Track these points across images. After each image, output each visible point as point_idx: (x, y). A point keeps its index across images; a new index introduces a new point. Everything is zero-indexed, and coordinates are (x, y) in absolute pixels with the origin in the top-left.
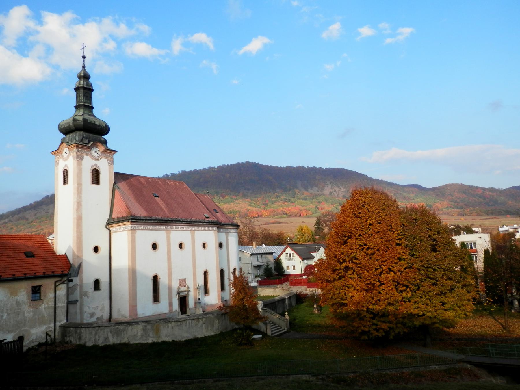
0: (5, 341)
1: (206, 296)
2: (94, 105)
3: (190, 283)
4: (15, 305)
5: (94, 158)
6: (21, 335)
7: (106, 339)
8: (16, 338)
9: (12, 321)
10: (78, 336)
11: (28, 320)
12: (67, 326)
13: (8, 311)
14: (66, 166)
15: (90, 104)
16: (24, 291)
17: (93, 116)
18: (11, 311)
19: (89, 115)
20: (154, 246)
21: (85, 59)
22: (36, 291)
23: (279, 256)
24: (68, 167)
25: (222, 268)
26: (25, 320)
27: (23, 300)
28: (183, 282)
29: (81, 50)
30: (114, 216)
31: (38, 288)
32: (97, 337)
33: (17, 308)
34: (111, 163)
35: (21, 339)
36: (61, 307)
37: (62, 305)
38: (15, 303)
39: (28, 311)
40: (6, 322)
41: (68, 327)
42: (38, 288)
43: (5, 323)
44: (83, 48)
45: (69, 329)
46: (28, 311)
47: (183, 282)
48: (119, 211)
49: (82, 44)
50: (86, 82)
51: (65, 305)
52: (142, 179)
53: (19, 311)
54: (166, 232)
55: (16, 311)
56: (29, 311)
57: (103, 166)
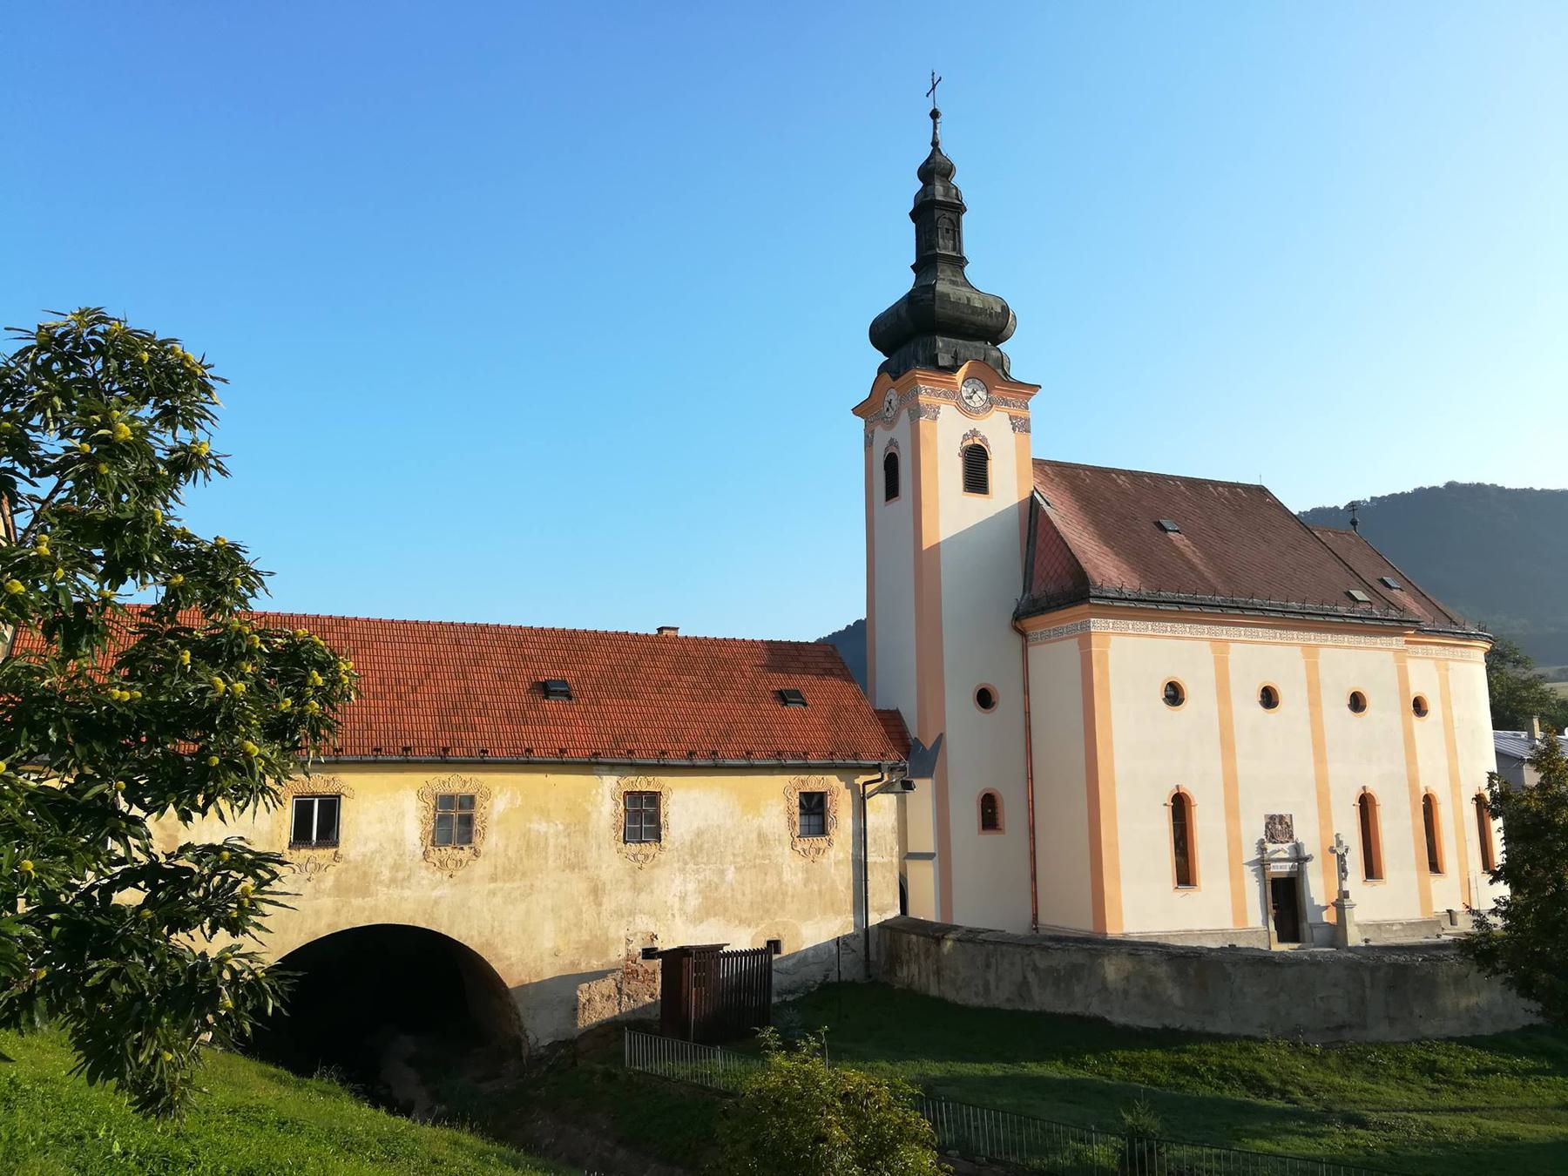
0: (726, 949)
1: (1001, 826)
2: (967, 251)
3: (1307, 834)
4: (755, 844)
5: (966, 410)
6: (775, 937)
7: (1023, 987)
8: (762, 945)
9: (748, 891)
10: (933, 964)
11: (790, 894)
12: (901, 927)
13: (738, 860)
14: (892, 442)
15: (954, 249)
16: (779, 805)
17: (967, 284)
18: (745, 860)
19: (954, 283)
20: (1174, 695)
21: (938, 120)
22: (814, 811)
23: (1410, 786)
24: (897, 447)
25: (979, 833)
26: (785, 894)
27: (776, 830)
28: (1278, 827)
29: (927, 96)
30: (1036, 593)
31: (816, 799)
32: (991, 977)
33: (761, 853)
34: (1021, 426)
35: (774, 945)
36: (883, 865)
37: (886, 860)
38: (754, 836)
39: (790, 866)
40: (733, 890)
41: (904, 931)
42: (816, 799)
43: (729, 895)
44: (933, 88)
45: (905, 937)
46: (790, 866)
47: (1278, 827)
48: (1051, 574)
49: (931, 77)
50: (943, 187)
51: (895, 860)
52: (1122, 477)
53: (767, 862)
54: (1211, 645)
55: (758, 861)
56: (793, 865)
57: (995, 429)
